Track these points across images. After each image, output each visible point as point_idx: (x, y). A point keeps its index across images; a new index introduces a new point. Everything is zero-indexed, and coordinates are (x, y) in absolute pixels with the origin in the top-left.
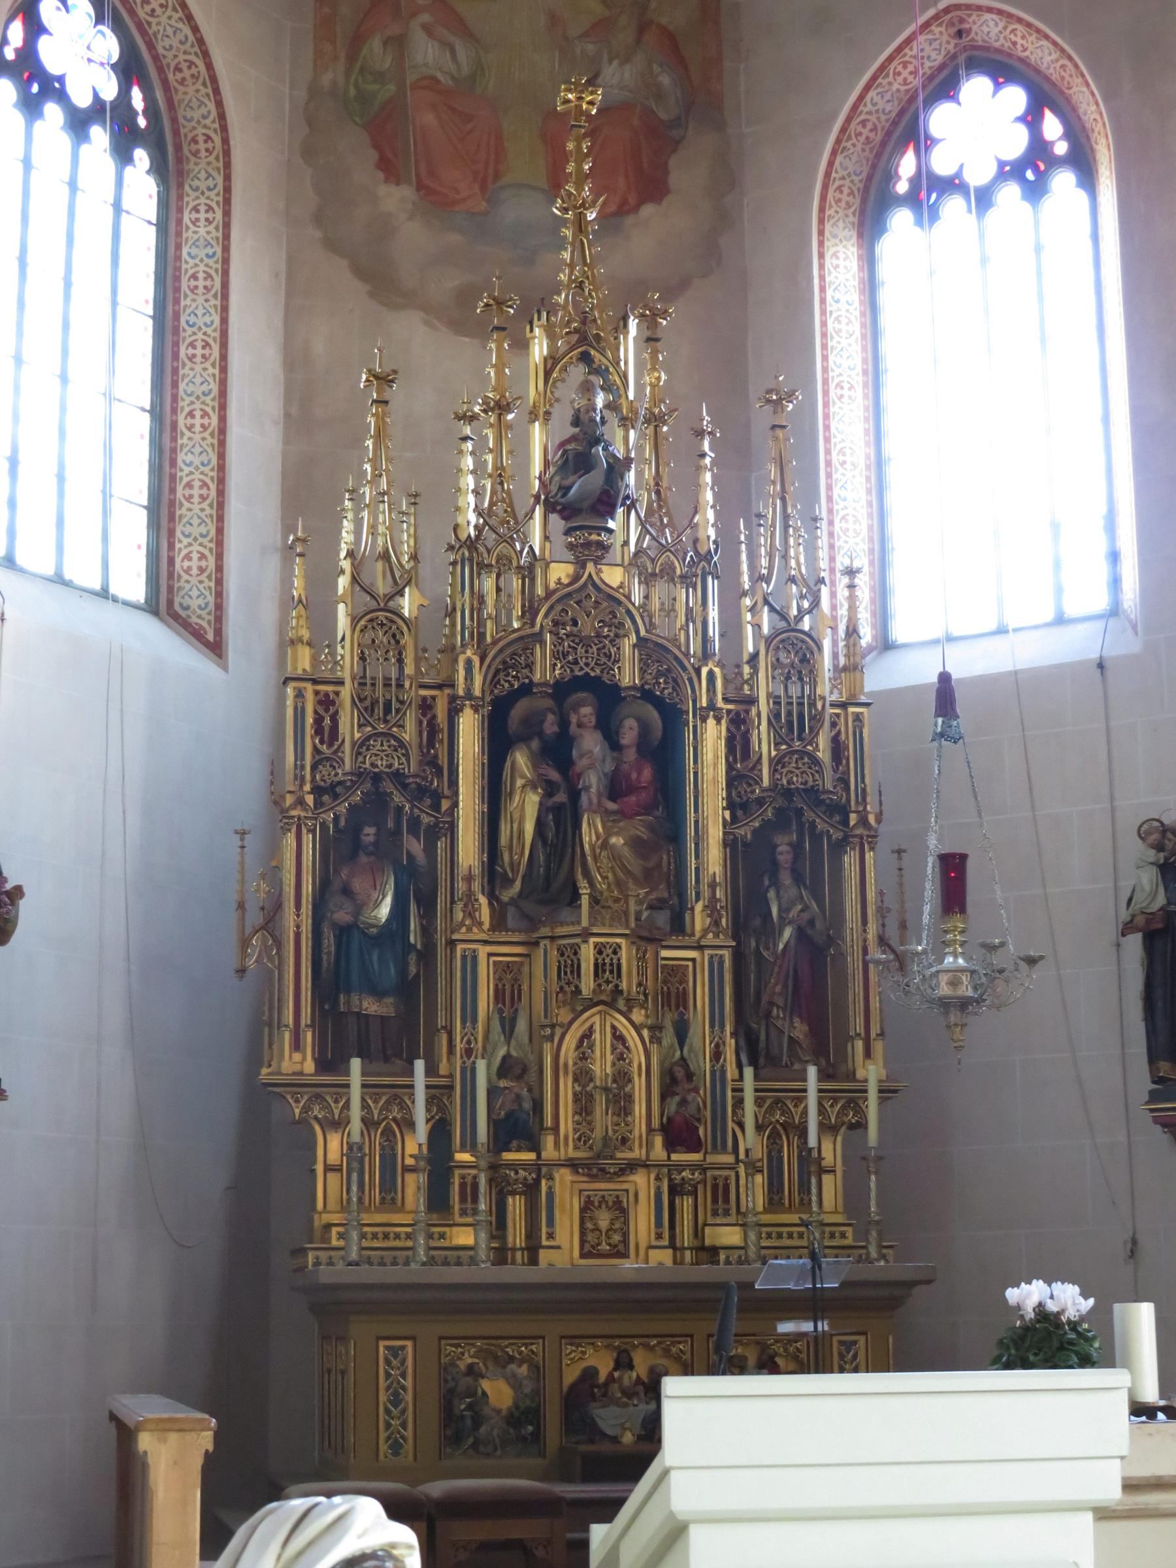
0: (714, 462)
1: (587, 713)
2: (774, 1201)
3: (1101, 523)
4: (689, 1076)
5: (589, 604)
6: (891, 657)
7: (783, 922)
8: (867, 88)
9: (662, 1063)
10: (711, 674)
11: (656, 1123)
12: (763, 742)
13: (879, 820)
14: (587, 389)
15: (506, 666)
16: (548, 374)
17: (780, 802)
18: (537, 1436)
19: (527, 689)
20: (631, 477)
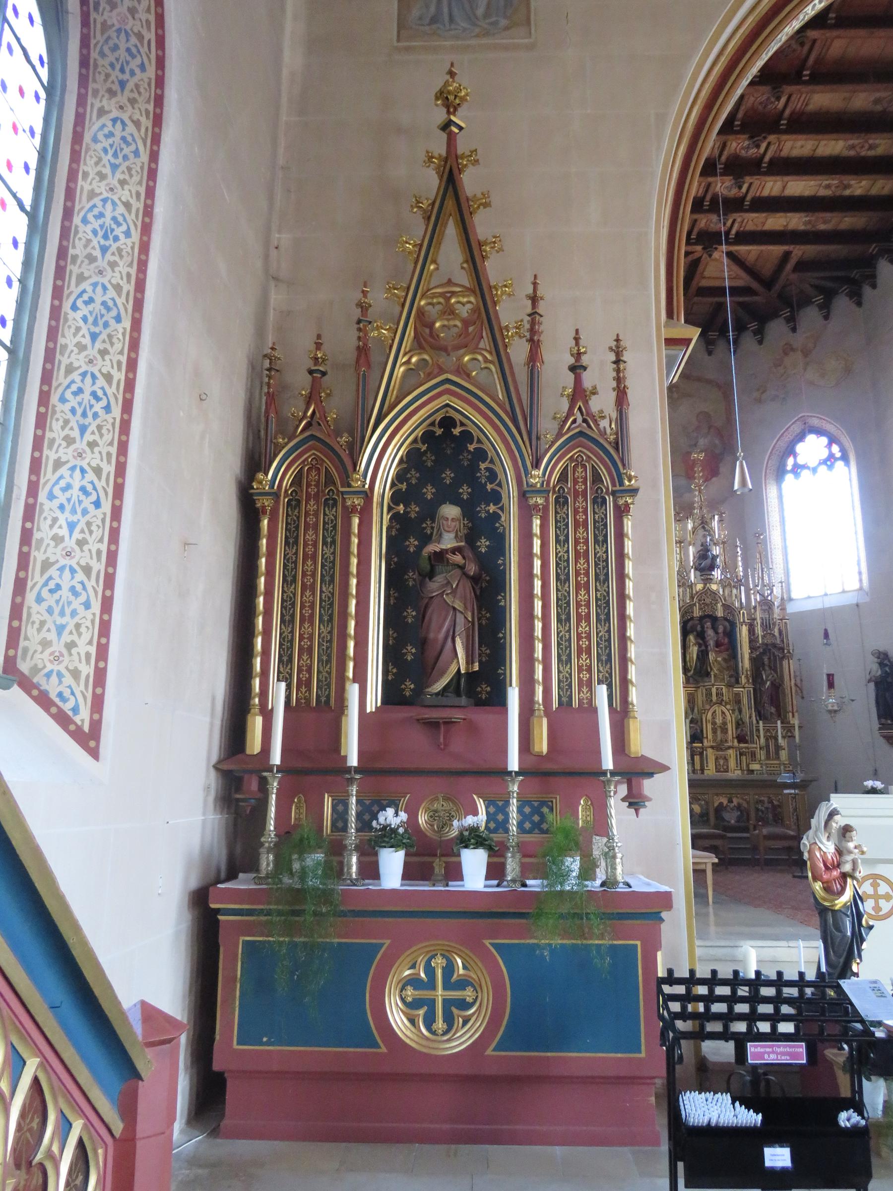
0: (741, 554)
1: (709, 624)
2: (768, 757)
3: (856, 563)
4: (743, 723)
5: (708, 595)
6: (792, 603)
7: (767, 680)
8: (778, 441)
9: (735, 719)
10: (743, 613)
11: (735, 736)
12: (759, 631)
13: (793, 650)
14: (705, 536)
15: (686, 612)
16: (693, 533)
17: (764, 647)
18: (708, 820)
19: (692, 618)
20: (718, 560)
